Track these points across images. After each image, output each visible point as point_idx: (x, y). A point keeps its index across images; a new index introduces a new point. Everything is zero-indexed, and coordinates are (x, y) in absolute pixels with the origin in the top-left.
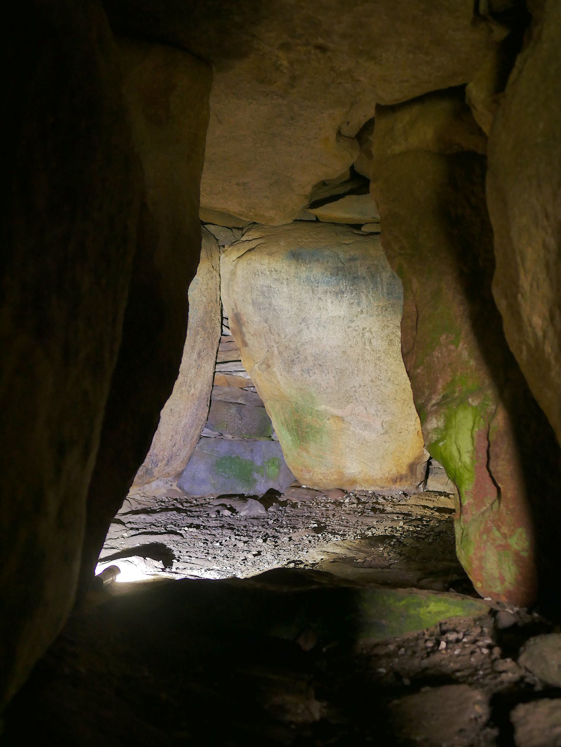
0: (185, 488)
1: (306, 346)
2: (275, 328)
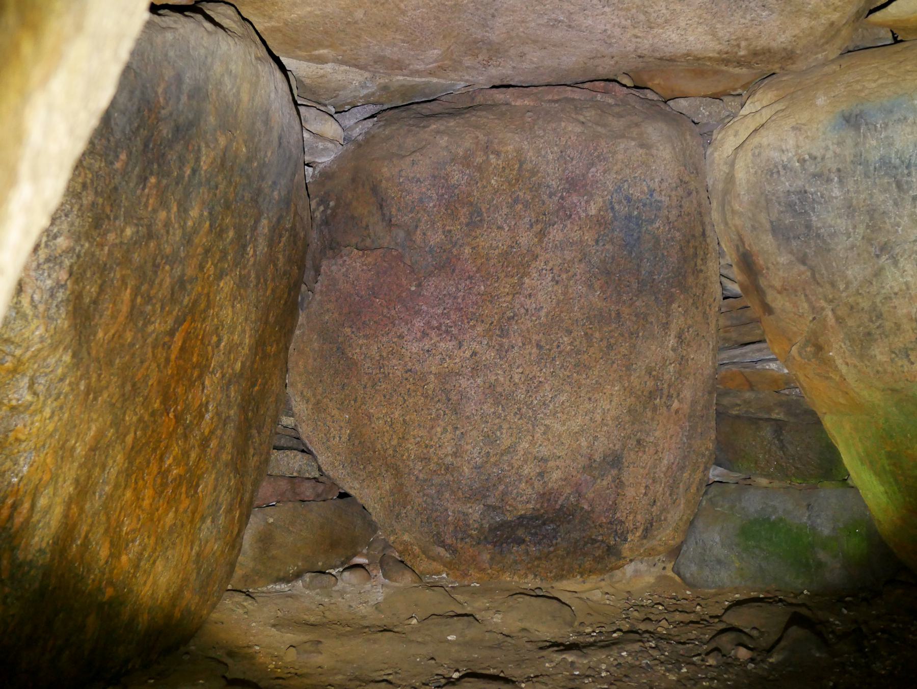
0: (688, 575)
1: (896, 302)
2: (824, 271)
